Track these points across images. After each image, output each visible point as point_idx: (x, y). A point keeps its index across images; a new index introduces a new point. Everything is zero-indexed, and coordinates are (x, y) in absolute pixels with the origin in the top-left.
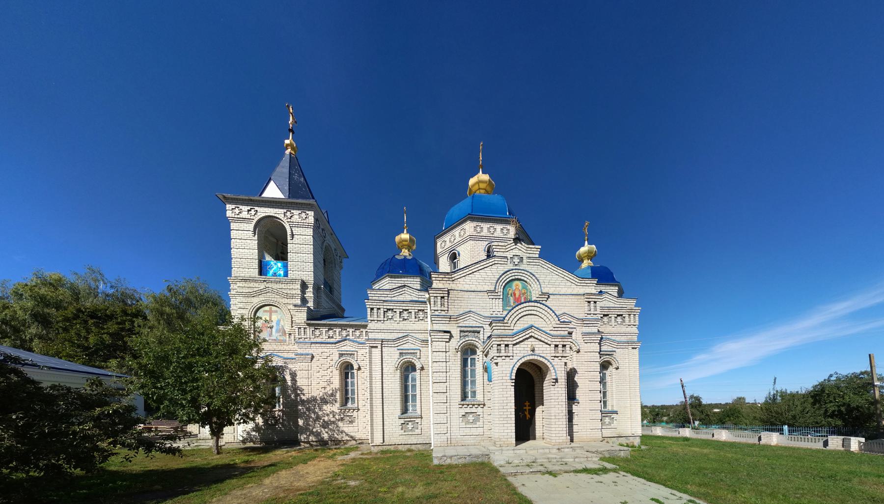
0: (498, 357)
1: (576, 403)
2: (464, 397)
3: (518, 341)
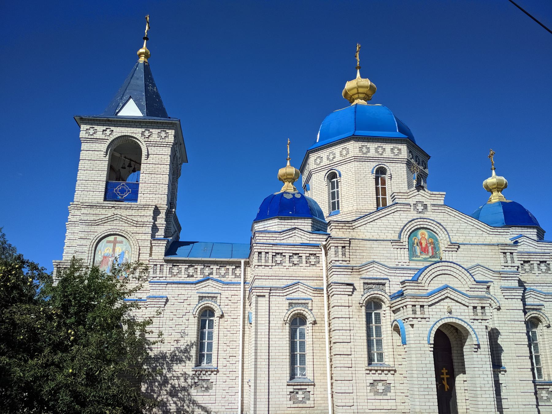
0: (413, 318)
1: (503, 371)
2: (370, 360)
3: (433, 302)
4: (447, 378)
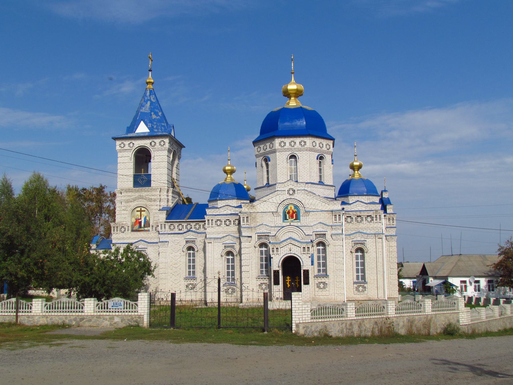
4: (289, 281)
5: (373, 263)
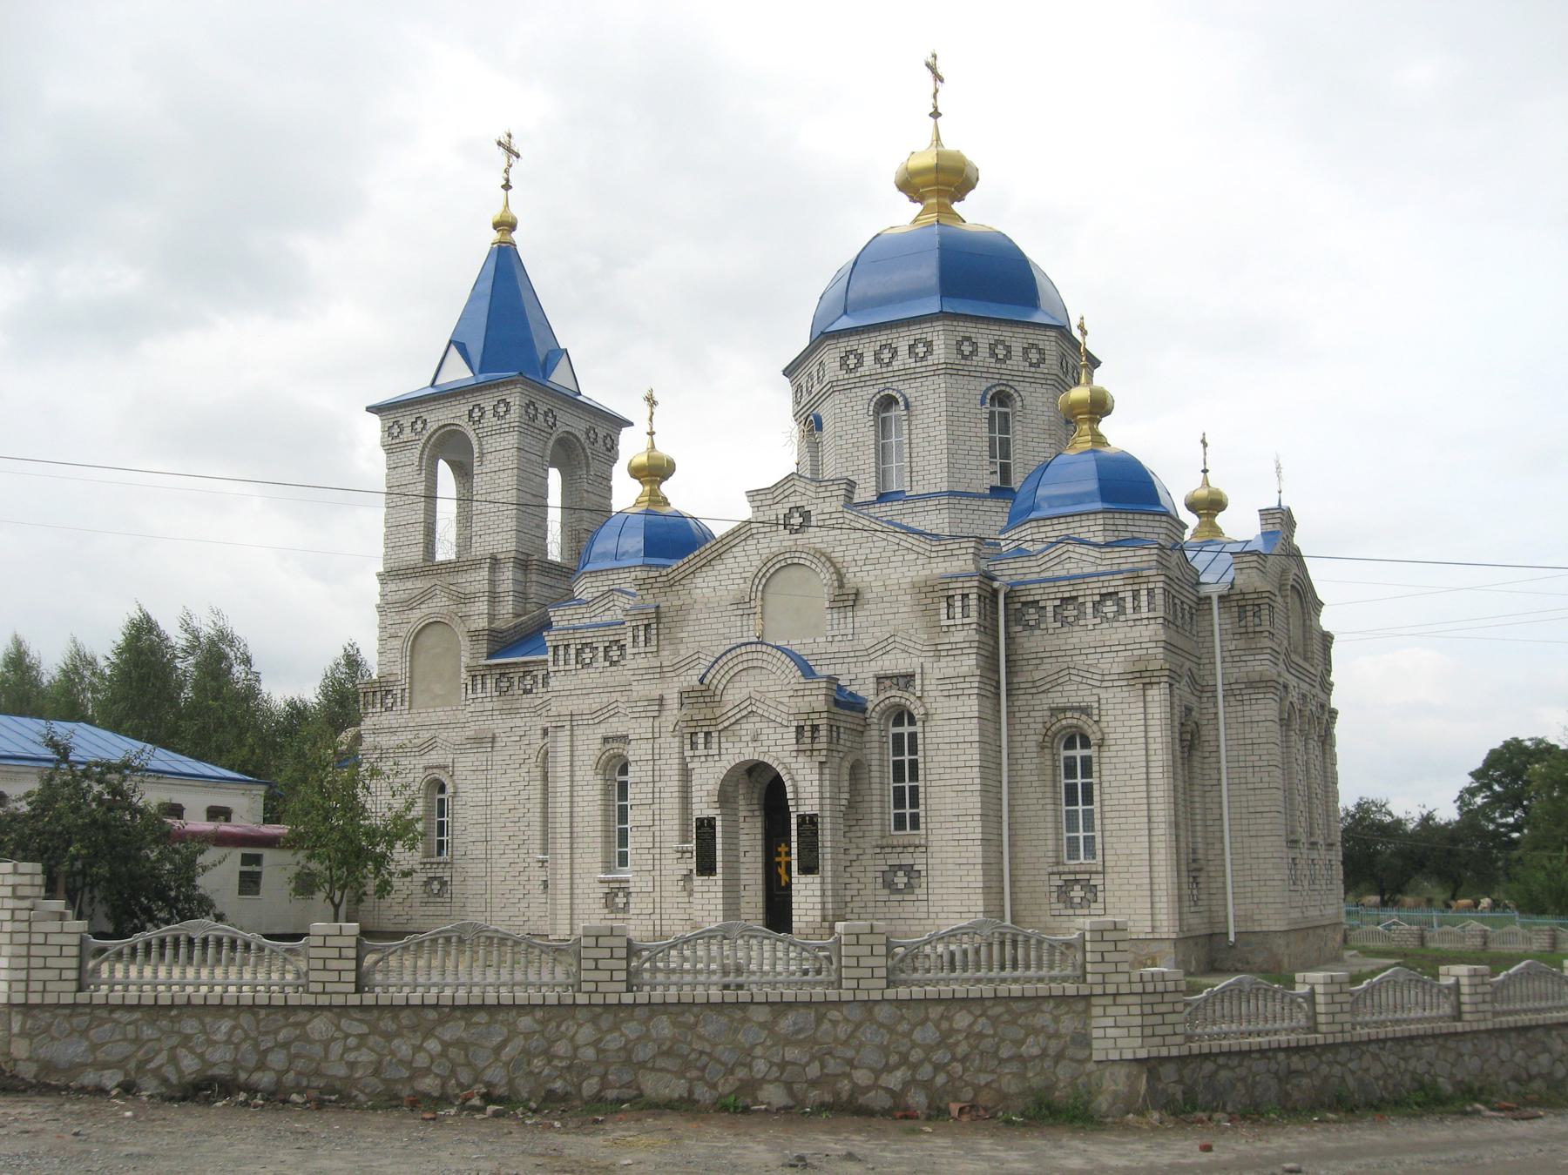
5: (1127, 789)
